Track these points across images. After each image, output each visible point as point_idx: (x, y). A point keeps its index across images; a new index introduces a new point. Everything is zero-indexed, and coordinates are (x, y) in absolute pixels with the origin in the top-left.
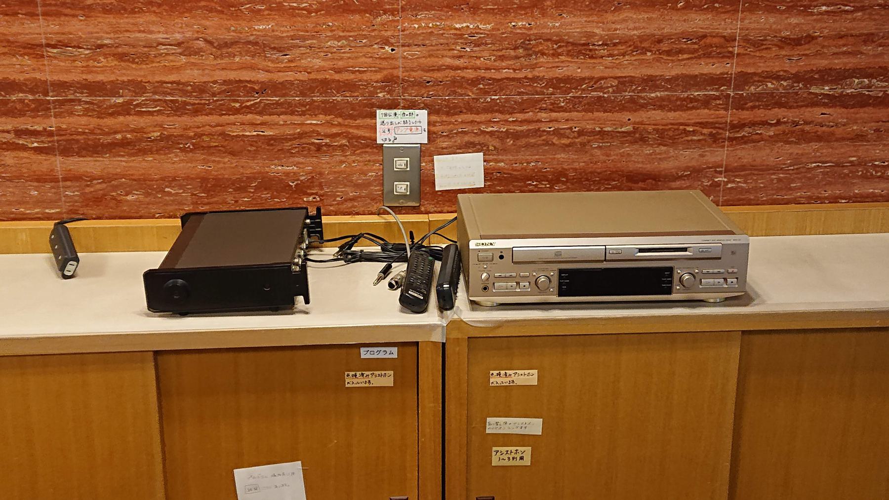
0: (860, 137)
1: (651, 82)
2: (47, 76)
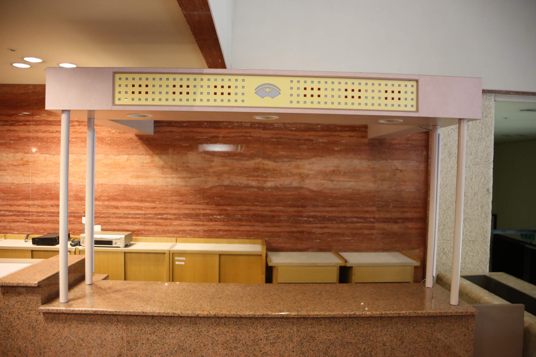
0: (167, 225)
1: (129, 214)
2: (31, 210)
